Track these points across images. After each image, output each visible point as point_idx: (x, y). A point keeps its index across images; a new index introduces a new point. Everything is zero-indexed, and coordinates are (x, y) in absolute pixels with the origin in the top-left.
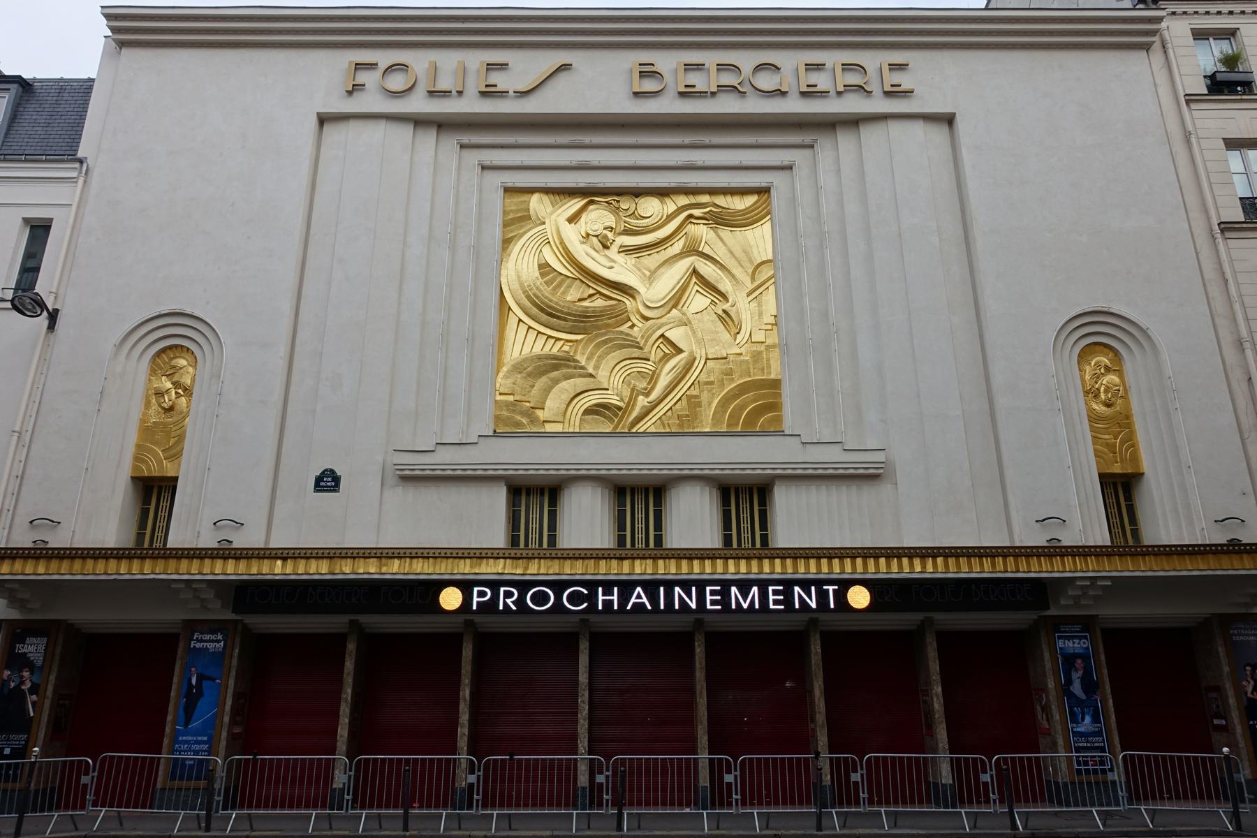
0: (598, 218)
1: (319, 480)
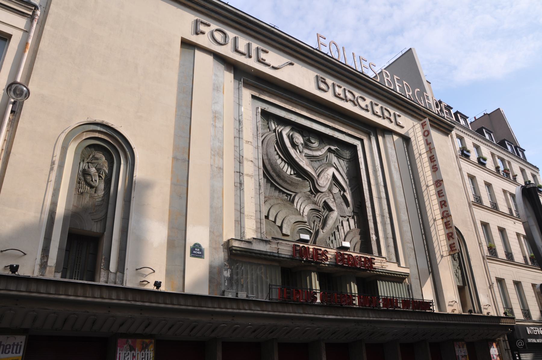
0: (299, 139)
1: (193, 249)
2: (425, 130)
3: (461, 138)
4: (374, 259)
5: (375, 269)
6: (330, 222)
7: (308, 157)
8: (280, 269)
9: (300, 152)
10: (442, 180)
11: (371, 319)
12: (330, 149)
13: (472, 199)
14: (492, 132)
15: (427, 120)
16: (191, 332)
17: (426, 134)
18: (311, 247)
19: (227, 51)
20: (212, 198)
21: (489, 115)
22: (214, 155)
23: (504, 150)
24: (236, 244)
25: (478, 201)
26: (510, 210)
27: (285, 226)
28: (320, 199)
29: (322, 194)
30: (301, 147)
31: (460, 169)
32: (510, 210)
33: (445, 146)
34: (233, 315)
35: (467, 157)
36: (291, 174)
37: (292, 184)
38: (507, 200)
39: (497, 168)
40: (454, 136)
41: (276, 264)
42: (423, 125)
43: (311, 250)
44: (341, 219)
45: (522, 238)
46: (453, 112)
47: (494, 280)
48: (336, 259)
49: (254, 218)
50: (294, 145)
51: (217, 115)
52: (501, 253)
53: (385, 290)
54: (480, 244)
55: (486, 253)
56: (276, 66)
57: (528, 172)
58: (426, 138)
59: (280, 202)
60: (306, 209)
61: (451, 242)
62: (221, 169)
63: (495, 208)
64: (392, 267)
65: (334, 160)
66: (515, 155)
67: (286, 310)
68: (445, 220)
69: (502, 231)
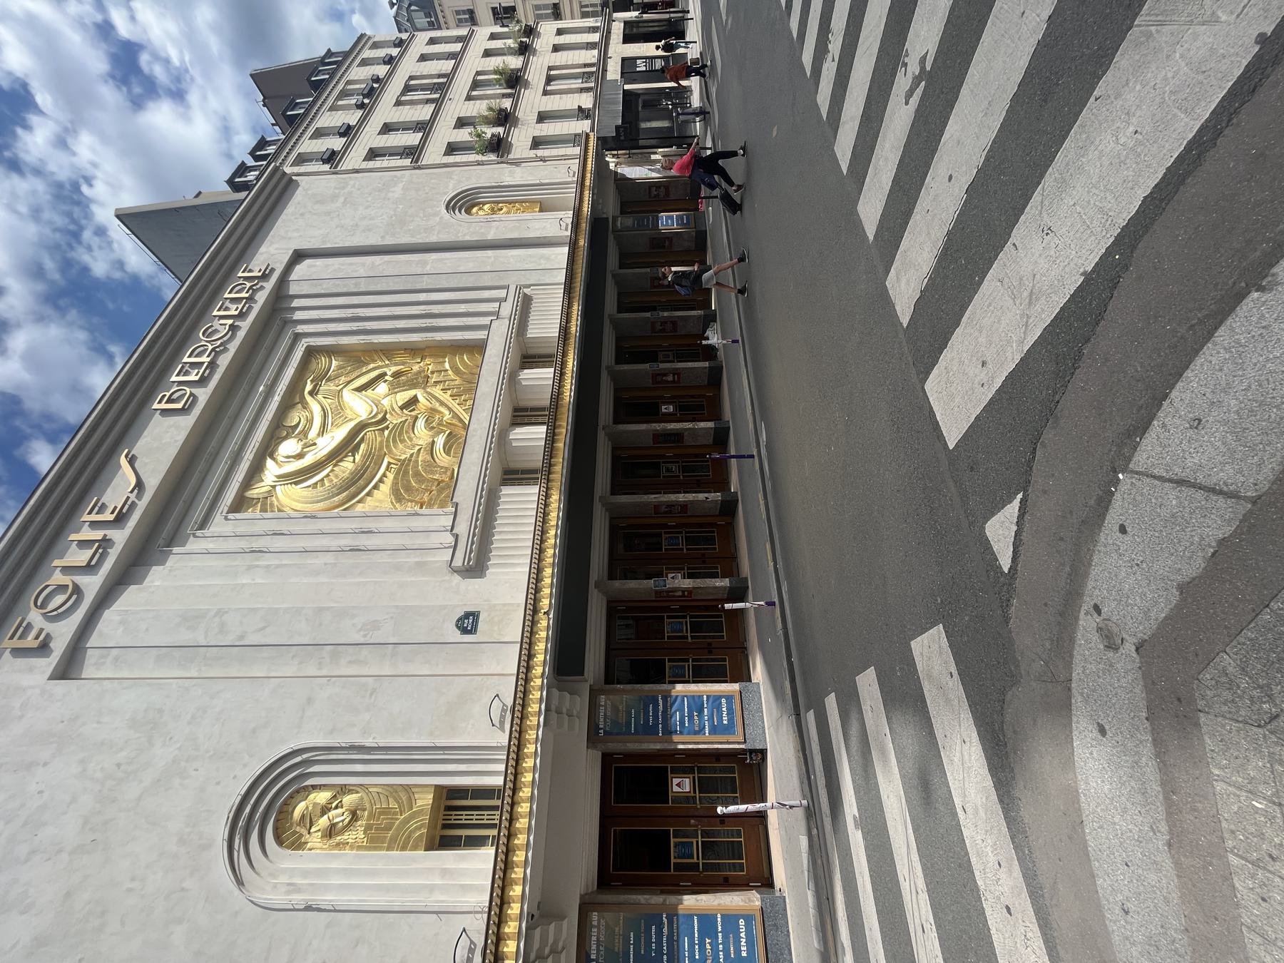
0: (289, 447)
1: (465, 631)
3: (302, 159)
7: (323, 430)
12: (311, 393)
13: (407, 162)
14: (293, 100)
19: (92, 584)
23: (327, 86)
25: (413, 153)
26: (428, 101)
31: (357, 171)
32: (428, 101)
35: (333, 153)
38: (412, 103)
39: (361, 106)
40: (296, 169)
45: (474, 93)
46: (250, 162)
47: (533, 153)
50: (300, 456)
52: (413, 139)
54: (479, 163)
57: (367, 54)
63: (424, 128)
69: (387, 129)
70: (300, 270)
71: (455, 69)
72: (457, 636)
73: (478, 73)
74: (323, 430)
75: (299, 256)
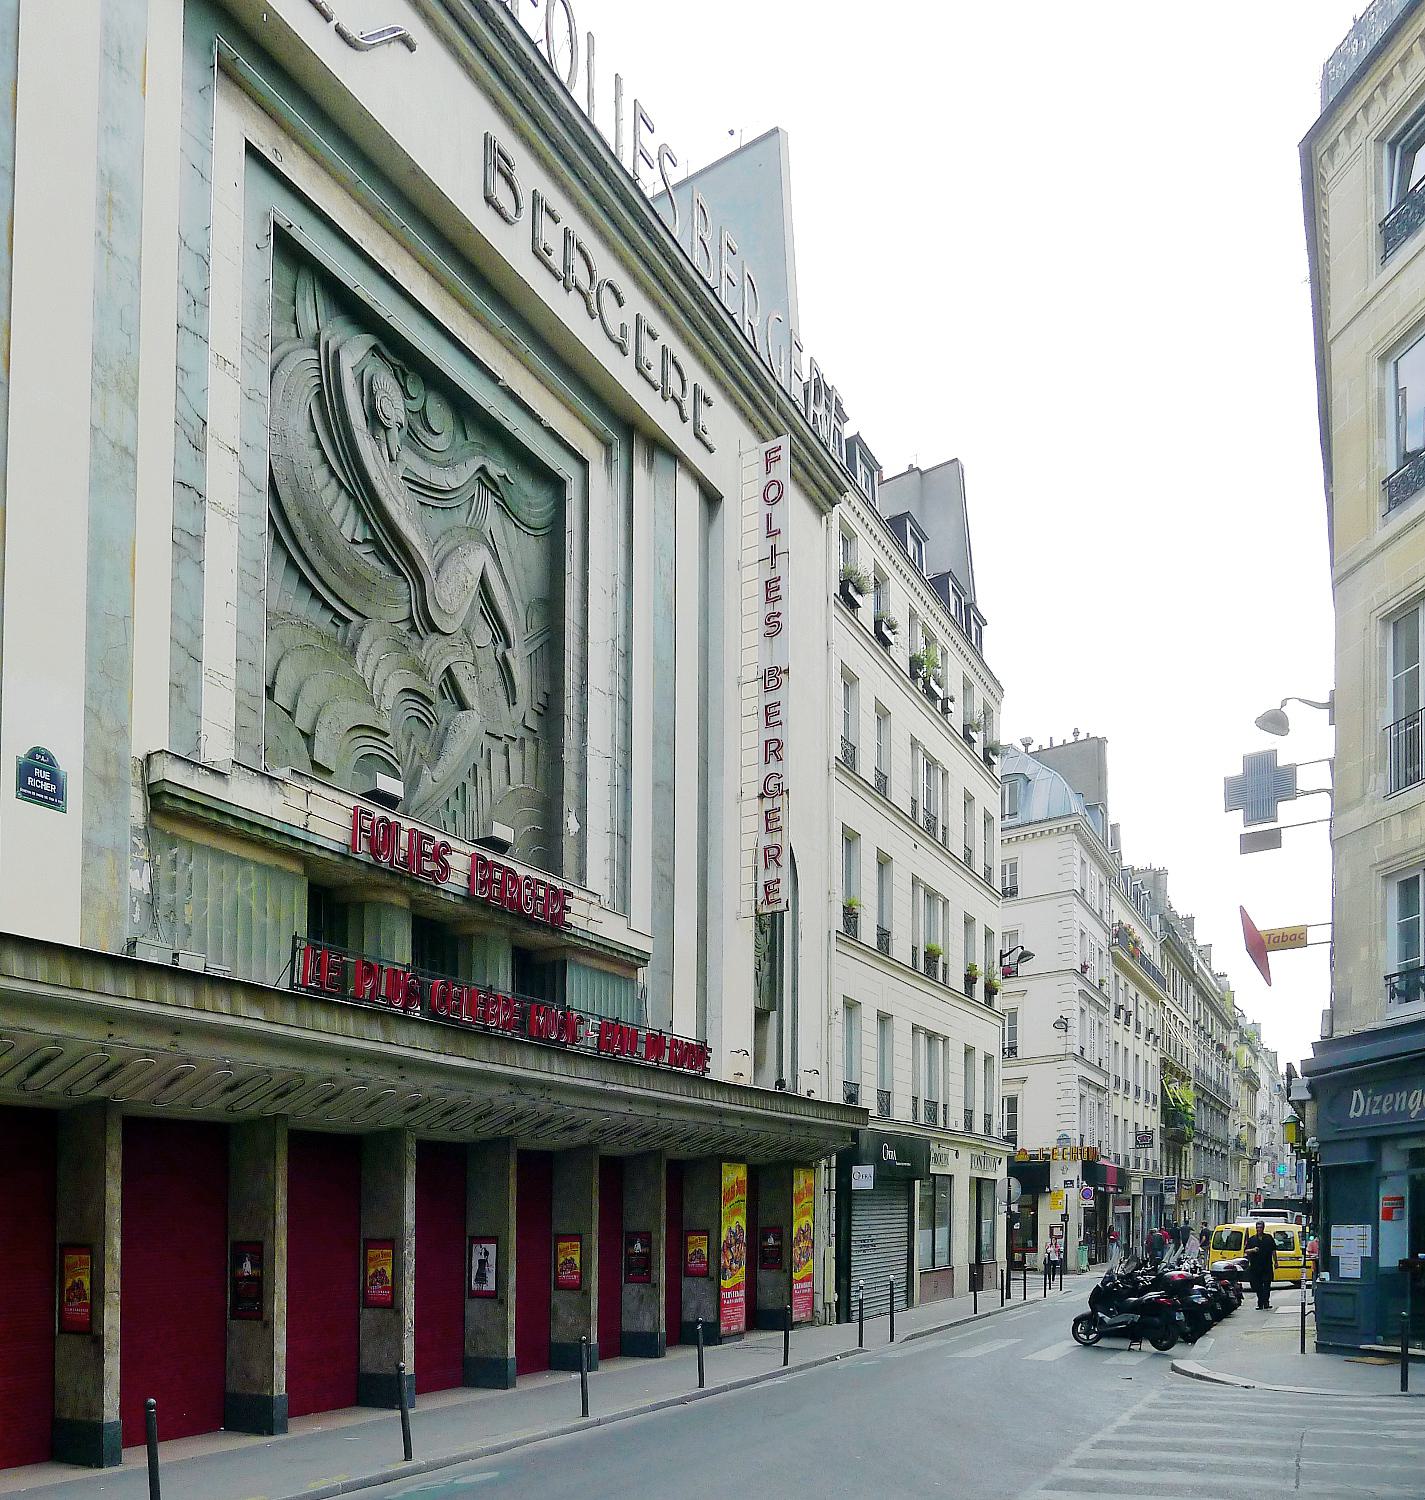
0: (394, 406)
2: (771, 477)
4: (570, 894)
5: (570, 925)
6: (457, 750)
7: (416, 484)
8: (306, 885)
9: (391, 460)
10: (787, 671)
11: (556, 1078)
12: (482, 469)
15: (784, 442)
16: (31, 1073)
17: (772, 496)
18: (407, 825)
20: (95, 572)
21: (922, 473)
22: (103, 385)
24: (176, 774)
27: (322, 735)
28: (436, 654)
29: (443, 641)
30: (395, 437)
33: (813, 548)
34: (177, 1028)
36: (354, 541)
37: (355, 578)
41: (295, 867)
42: (770, 459)
43: (404, 836)
44: (487, 742)
48: (469, 878)
49: (231, 684)
50: (374, 419)
51: (116, 196)
53: (583, 992)
55: (838, 924)
56: (353, 33)
57: (979, 693)
58: (768, 509)
59: (312, 641)
60: (391, 682)
61: (771, 875)
62: (128, 454)
64: (612, 929)
65: (493, 519)
66: (960, 628)
67: (671, 1090)
68: (768, 804)
70: (688, 496)
71: (952, 857)
72: (17, 749)
73: (946, 902)
74: (416, 484)
75: (711, 499)
